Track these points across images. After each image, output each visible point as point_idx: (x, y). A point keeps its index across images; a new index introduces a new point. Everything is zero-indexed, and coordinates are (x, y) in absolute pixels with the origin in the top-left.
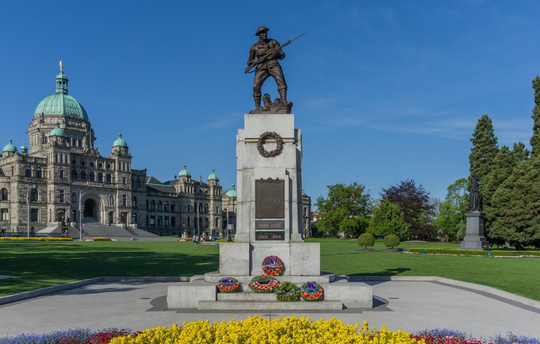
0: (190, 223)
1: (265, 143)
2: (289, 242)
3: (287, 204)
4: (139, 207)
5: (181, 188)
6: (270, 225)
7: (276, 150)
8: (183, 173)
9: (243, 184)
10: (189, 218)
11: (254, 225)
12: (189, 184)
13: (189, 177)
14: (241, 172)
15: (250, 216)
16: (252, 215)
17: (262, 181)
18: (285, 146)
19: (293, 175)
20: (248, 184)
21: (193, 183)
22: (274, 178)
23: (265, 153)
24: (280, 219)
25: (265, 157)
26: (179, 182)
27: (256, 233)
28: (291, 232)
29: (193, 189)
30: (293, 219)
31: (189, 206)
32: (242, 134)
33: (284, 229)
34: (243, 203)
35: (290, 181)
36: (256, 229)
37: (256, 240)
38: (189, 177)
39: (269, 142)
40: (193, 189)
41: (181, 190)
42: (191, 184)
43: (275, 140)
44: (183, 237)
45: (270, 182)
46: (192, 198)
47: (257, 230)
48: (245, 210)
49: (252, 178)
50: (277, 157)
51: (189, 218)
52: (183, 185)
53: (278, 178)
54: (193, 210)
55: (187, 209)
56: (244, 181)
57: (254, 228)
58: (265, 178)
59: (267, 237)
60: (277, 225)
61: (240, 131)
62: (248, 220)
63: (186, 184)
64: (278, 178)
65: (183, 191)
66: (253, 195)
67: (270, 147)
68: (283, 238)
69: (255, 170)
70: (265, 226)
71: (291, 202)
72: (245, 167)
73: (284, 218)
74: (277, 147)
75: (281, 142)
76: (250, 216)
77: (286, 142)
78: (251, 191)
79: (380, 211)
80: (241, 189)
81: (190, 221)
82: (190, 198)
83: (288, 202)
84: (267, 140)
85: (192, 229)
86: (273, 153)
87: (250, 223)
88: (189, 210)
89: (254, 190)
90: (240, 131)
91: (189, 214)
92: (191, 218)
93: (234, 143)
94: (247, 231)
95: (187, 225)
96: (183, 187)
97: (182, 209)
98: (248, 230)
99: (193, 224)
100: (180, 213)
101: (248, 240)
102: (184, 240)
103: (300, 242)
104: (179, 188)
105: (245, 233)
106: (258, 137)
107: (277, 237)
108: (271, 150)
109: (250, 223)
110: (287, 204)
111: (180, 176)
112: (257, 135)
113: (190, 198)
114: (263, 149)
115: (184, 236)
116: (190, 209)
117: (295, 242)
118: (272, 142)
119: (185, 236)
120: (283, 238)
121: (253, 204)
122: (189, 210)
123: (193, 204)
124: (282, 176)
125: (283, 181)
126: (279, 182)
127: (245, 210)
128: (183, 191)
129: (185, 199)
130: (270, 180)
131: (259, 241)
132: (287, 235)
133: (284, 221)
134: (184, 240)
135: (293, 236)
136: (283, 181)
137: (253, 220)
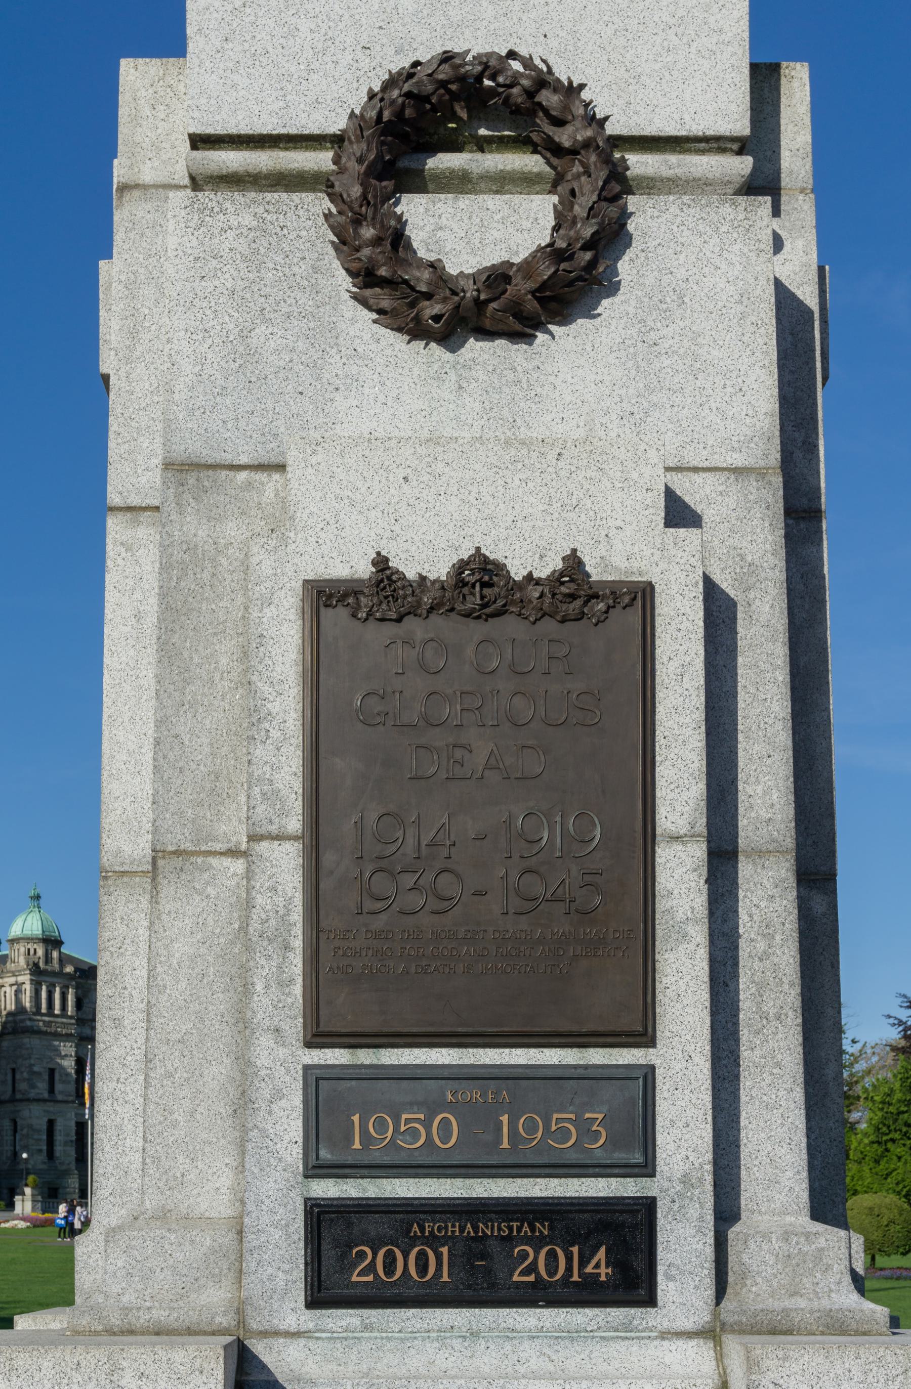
0: (58, 1149)
1: (416, 182)
2: (712, 1334)
3: (680, 876)
4: (60, 1097)
5: (17, 993)
6: (478, 1118)
7: (555, 253)
8: (28, 924)
9: (167, 653)
10: (51, 1123)
11: (285, 1125)
12: (53, 974)
13: (52, 942)
14: (145, 534)
15: (243, 1024)
16: (263, 1003)
17: (385, 592)
18: (645, 216)
19: (745, 541)
20: (225, 654)
21: (69, 969)
22: (528, 557)
23: (422, 279)
24: (597, 1056)
25: (417, 331)
26: (10, 966)
27: (320, 1219)
28: (726, 1212)
29: (71, 998)
30: (750, 1054)
31: (52, 1072)
32: (157, 111)
33: (647, 1168)
34: (165, 862)
35: (719, 615)
36: (315, 1169)
37: (313, 1303)
38: (52, 942)
39: (460, 183)
40: (71, 998)
41: (18, 1001)
42: (60, 974)
43: (531, 162)
44: (18, 1209)
45: (488, 612)
46: (68, 1037)
47: (328, 1189)
48: (182, 948)
49: (264, 561)
50: (564, 347)
51: (51, 1123)
52: (25, 978)
53: (574, 562)
54: (72, 1088)
55: (42, 1087)
56: (174, 611)
57: (294, 1155)
58: (427, 558)
59: (442, 1267)
60: (562, 1117)
61: (136, 76)
62: (218, 1071)
63: (36, 971)
64: (574, 562)
65: (27, 1003)
66: (284, 767)
67: (485, 222)
68: (632, 1282)
69: (305, 485)
70: (414, 1131)
71: (722, 857)
72: (191, 445)
73: (645, 1036)
74: (561, 221)
75: (597, 176)
76: (243, 1024)
77: (652, 186)
78: (254, 718)
79: (898, 1095)
80: (148, 711)
81: (59, 1138)
82: (56, 1035)
83: (698, 851)
84: (442, 162)
85: (66, 1173)
86: (520, 287)
87: (243, 1105)
88: (52, 1090)
89: (286, 707)
90: (136, 76)
91: (50, 1107)
92: (59, 1127)
93: (79, 211)
94: (212, 1195)
95: (43, 1157)
96: (27, 987)
97: (22, 1086)
98: (225, 1180)
99: (72, 1152)
100: (13, 1100)
101: (214, 1300)
102: (22, 1225)
103: (836, 1327)
104: (10, 992)
105: (187, 1221)
106: (337, 124)
107: (565, 1263)
108: (493, 257)
109: (243, 1105)
110: (680, 876)
111: (13, 941)
112: (333, 96)
113: (56, 1035)
114: (397, 239)
115: (25, 1204)
116: (58, 1087)
117: (778, 1328)
118: (502, 183)
119: (28, 1205)
120: (632, 1282)
121: (285, 865)
122: (52, 1090)
123: (69, 1064)
124: (624, 545)
125: (642, 596)
126: (588, 611)
127: (182, 948)
128: (27, 1003)
129: (34, 1042)
130: (480, 585)
131: (349, 1318)
132: (682, 1245)
133: (648, 1074)
134: (22, 1225)
135: (752, 1251)
136: (642, 596)
137: (284, 1061)
